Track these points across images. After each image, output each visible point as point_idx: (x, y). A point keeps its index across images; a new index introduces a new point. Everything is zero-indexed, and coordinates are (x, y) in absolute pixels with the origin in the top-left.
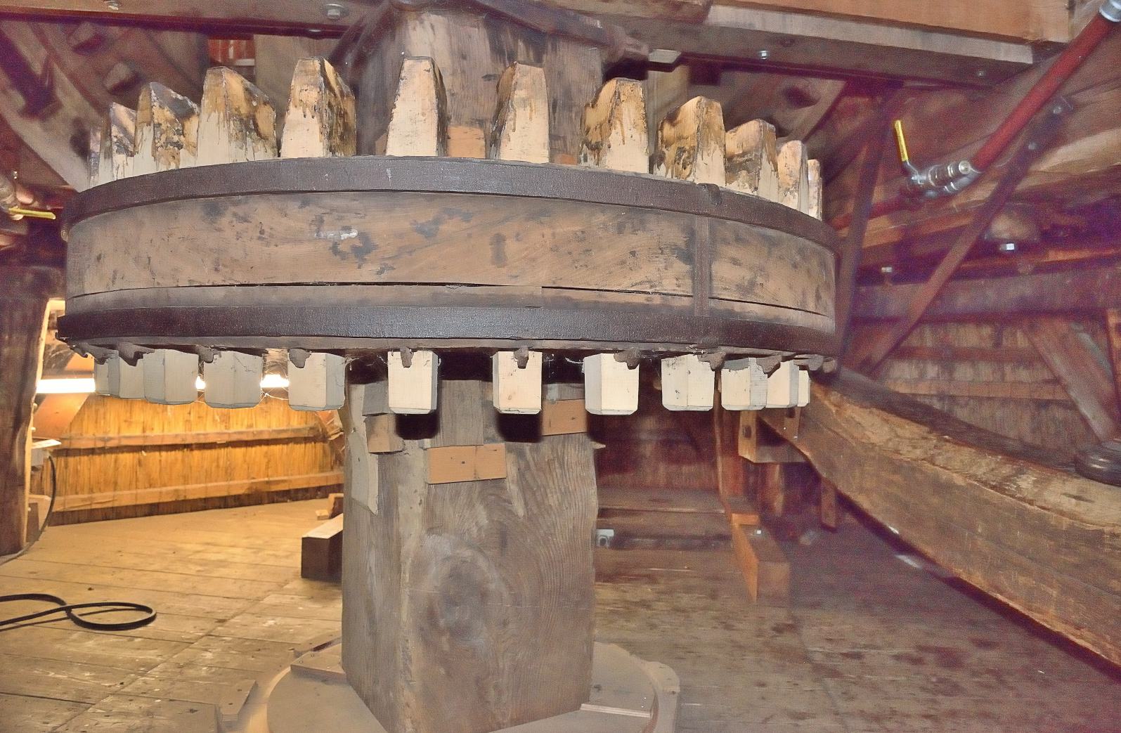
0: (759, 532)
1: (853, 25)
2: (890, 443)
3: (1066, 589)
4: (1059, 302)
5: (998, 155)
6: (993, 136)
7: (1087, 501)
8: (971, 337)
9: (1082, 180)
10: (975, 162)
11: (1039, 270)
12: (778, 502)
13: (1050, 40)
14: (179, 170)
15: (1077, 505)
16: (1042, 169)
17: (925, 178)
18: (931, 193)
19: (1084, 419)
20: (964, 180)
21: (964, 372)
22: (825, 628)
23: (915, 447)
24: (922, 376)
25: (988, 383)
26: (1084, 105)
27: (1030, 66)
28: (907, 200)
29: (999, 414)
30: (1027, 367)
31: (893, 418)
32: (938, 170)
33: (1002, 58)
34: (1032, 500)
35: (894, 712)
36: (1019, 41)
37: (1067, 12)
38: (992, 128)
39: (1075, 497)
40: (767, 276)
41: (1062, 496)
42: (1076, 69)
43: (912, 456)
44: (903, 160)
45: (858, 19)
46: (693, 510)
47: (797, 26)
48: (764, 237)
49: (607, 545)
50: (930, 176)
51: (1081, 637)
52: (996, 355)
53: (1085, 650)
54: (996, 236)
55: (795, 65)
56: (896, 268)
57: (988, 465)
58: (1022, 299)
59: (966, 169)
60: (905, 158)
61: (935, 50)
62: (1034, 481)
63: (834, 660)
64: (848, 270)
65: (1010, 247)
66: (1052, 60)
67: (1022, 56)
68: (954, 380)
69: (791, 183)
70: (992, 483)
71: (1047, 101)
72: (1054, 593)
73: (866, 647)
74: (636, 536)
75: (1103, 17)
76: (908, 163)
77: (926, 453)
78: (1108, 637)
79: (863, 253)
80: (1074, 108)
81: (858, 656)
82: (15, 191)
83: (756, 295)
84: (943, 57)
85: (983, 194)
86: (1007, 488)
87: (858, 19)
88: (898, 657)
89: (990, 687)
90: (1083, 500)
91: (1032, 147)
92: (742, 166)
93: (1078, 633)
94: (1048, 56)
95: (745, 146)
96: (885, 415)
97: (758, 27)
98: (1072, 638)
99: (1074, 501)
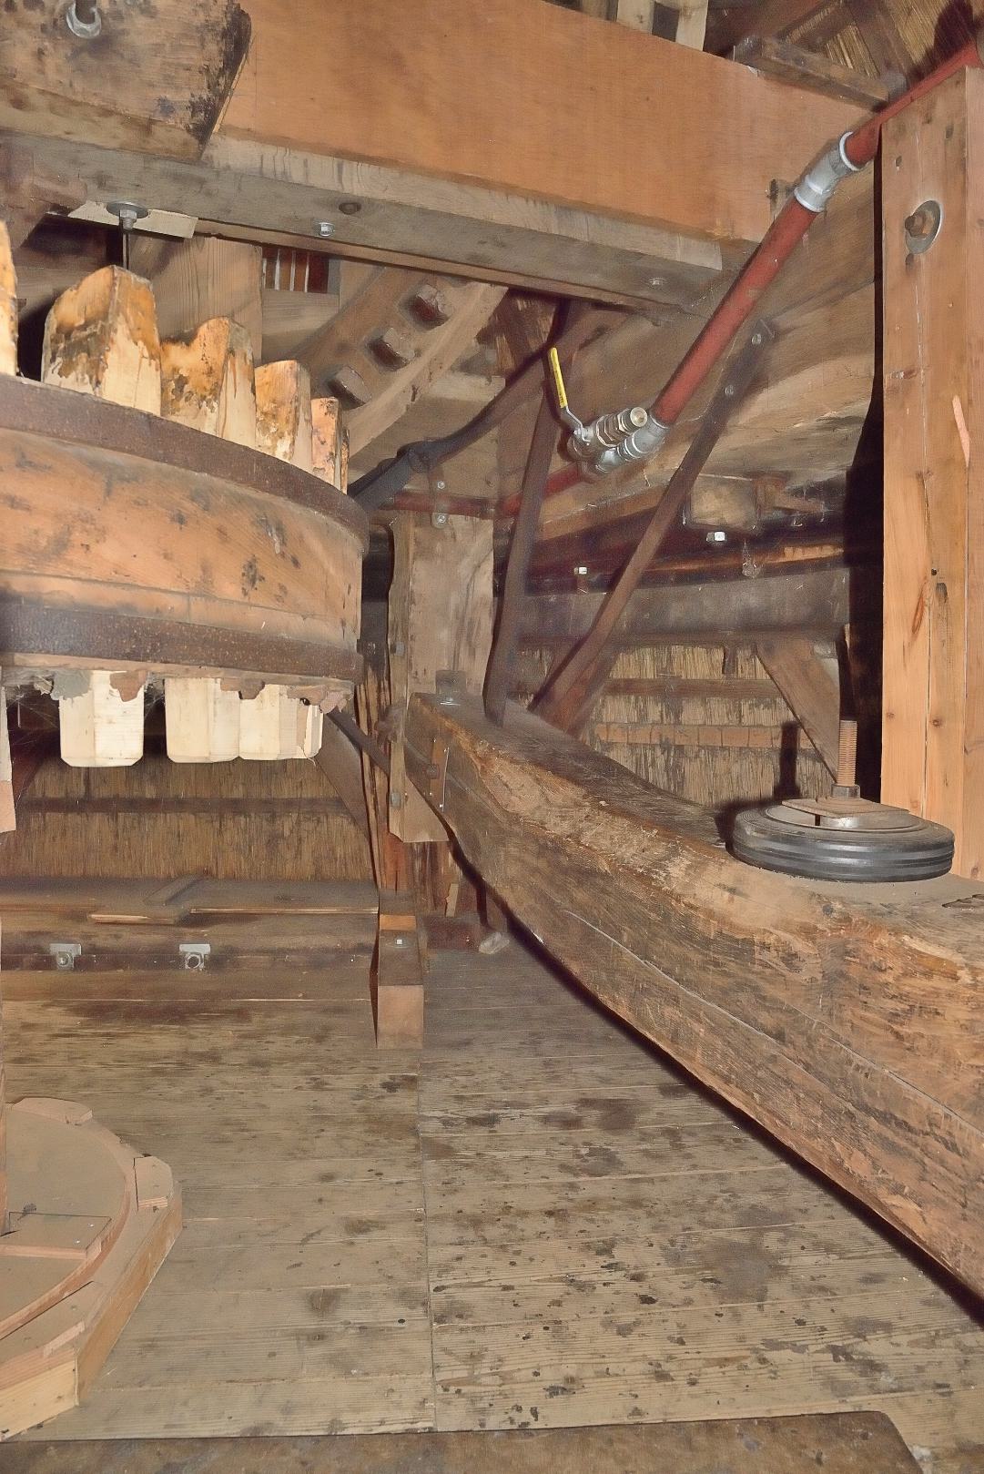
2: (538, 814)
4: (788, 614)
8: (699, 664)
11: (770, 572)
13: (746, 237)
16: (741, 422)
21: (693, 713)
22: (462, 1079)
23: (563, 818)
24: (643, 716)
25: (721, 728)
26: (788, 331)
29: (735, 769)
30: (768, 706)
31: (548, 777)
33: (679, 256)
34: (680, 895)
35: (507, 1209)
37: (769, 201)
40: (103, 533)
43: (558, 831)
46: (334, 910)
47: (359, 182)
48: (95, 465)
49: (201, 966)
51: (731, 1094)
52: (730, 690)
53: (739, 1110)
54: (698, 521)
57: (640, 842)
58: (748, 611)
60: (564, 403)
62: (689, 867)
63: (454, 1129)
65: (720, 537)
68: (680, 723)
69: (208, 387)
73: (508, 1105)
74: (243, 952)
77: (574, 826)
78: (756, 1096)
79: (539, 549)
80: (775, 335)
81: (489, 1121)
83: (70, 563)
84: (592, 248)
86: (655, 876)
87: (459, 179)
88: (546, 1120)
89: (661, 1157)
91: (729, 391)
92: (81, 346)
93: (727, 1088)
95: (89, 310)
96: (539, 772)
97: (297, 176)
98: (724, 1095)
99: (727, 894)
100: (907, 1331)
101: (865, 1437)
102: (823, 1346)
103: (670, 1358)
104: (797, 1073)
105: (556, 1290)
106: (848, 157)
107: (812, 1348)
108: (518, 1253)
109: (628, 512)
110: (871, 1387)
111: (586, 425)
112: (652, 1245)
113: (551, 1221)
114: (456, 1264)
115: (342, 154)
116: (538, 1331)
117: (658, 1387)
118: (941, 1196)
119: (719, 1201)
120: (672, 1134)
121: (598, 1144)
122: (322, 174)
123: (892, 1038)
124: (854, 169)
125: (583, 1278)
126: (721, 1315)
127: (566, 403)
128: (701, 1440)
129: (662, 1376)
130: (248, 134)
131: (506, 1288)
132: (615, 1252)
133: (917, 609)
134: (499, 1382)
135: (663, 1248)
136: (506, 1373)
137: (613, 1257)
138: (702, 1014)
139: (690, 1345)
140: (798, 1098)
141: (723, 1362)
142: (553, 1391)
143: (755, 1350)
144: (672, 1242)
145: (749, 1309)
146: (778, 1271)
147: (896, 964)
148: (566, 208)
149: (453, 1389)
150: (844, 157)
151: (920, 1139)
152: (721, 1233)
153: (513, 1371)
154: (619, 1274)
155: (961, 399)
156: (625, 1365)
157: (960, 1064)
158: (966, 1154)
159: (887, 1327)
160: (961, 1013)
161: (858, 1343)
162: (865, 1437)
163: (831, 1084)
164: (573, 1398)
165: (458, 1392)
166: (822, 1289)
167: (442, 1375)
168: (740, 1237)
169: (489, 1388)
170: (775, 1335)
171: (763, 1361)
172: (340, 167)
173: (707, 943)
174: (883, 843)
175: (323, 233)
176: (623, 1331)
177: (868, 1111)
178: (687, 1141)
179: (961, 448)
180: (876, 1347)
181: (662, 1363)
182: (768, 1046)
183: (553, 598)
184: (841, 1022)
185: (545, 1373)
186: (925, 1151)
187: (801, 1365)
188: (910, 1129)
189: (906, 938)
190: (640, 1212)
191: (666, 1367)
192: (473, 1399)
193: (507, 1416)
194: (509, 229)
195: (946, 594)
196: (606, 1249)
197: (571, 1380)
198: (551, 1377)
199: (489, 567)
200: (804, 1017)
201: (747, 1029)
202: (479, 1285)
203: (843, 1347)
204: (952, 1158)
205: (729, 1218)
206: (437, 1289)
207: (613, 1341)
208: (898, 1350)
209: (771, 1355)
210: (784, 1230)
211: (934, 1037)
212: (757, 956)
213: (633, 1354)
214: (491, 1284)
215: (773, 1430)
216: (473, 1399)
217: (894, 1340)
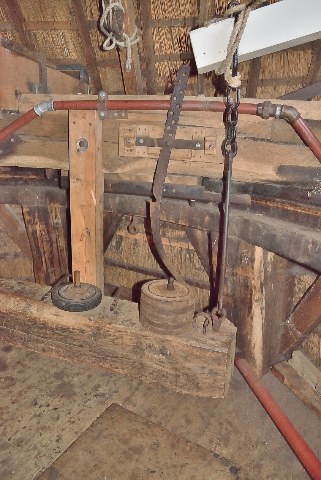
3: (59, 347)
7: (60, 316)
9: (288, 268)
14: (169, 159)
15: (57, 318)
37: (15, 96)
39: (55, 315)
41: (50, 315)
70: (19, 311)
72: (54, 348)
80: (19, 141)
86: (27, 313)
90: (58, 316)
99: (55, 317)
100: (103, 384)
101: (115, 409)
102: (93, 397)
103: (71, 418)
104: (87, 353)
105: (35, 420)
107: (92, 398)
108: (17, 418)
110: (106, 399)
112: (44, 396)
113: (16, 404)
114: (6, 431)
116: (42, 432)
117: (74, 425)
118: (127, 367)
119: (47, 376)
120: (19, 363)
121: (4, 376)
123: (112, 343)
125: (38, 413)
126: (72, 403)
128: (93, 429)
129: (73, 423)
131: (24, 428)
132: (38, 402)
133: (82, 236)
134: (45, 448)
135: (47, 395)
136: (45, 444)
137: (39, 404)
138: (53, 344)
139: (72, 413)
140: (88, 357)
141: (80, 412)
142: (57, 441)
143: (83, 405)
144: (47, 392)
145: (75, 398)
146: (73, 386)
147: (113, 331)
149: (38, 457)
151: (121, 359)
152: (55, 384)
153: (46, 443)
154: (44, 407)
155: (94, 191)
156: (65, 426)
157: (129, 345)
158: (132, 359)
159: (99, 385)
160: (129, 337)
161: (98, 392)
162: (115, 409)
163: (98, 353)
164: (62, 439)
165: (40, 456)
166: (84, 384)
167: (33, 456)
168: (59, 382)
169: (45, 451)
170: (84, 400)
171: (86, 406)
173: (53, 329)
176: (58, 419)
177: (108, 356)
178: (25, 363)
179: (94, 202)
180: (101, 391)
181: (71, 420)
182: (78, 348)
184: (99, 342)
185: (52, 439)
186: (122, 360)
187: (93, 403)
188: (119, 358)
189: (113, 325)
190: (33, 389)
191: (72, 420)
192: (45, 455)
193: (54, 453)
195: (90, 234)
196: (36, 404)
197: (58, 436)
198: (54, 438)
200: (88, 342)
201: (70, 346)
202: (17, 432)
203: (96, 394)
204: (129, 361)
205: (53, 379)
206: (9, 440)
207: (57, 423)
208: (104, 389)
209: (87, 404)
210: (66, 375)
211: (123, 342)
212: (71, 331)
213: (64, 422)
214: (20, 429)
215: (102, 418)
216: (45, 455)
217: (102, 387)
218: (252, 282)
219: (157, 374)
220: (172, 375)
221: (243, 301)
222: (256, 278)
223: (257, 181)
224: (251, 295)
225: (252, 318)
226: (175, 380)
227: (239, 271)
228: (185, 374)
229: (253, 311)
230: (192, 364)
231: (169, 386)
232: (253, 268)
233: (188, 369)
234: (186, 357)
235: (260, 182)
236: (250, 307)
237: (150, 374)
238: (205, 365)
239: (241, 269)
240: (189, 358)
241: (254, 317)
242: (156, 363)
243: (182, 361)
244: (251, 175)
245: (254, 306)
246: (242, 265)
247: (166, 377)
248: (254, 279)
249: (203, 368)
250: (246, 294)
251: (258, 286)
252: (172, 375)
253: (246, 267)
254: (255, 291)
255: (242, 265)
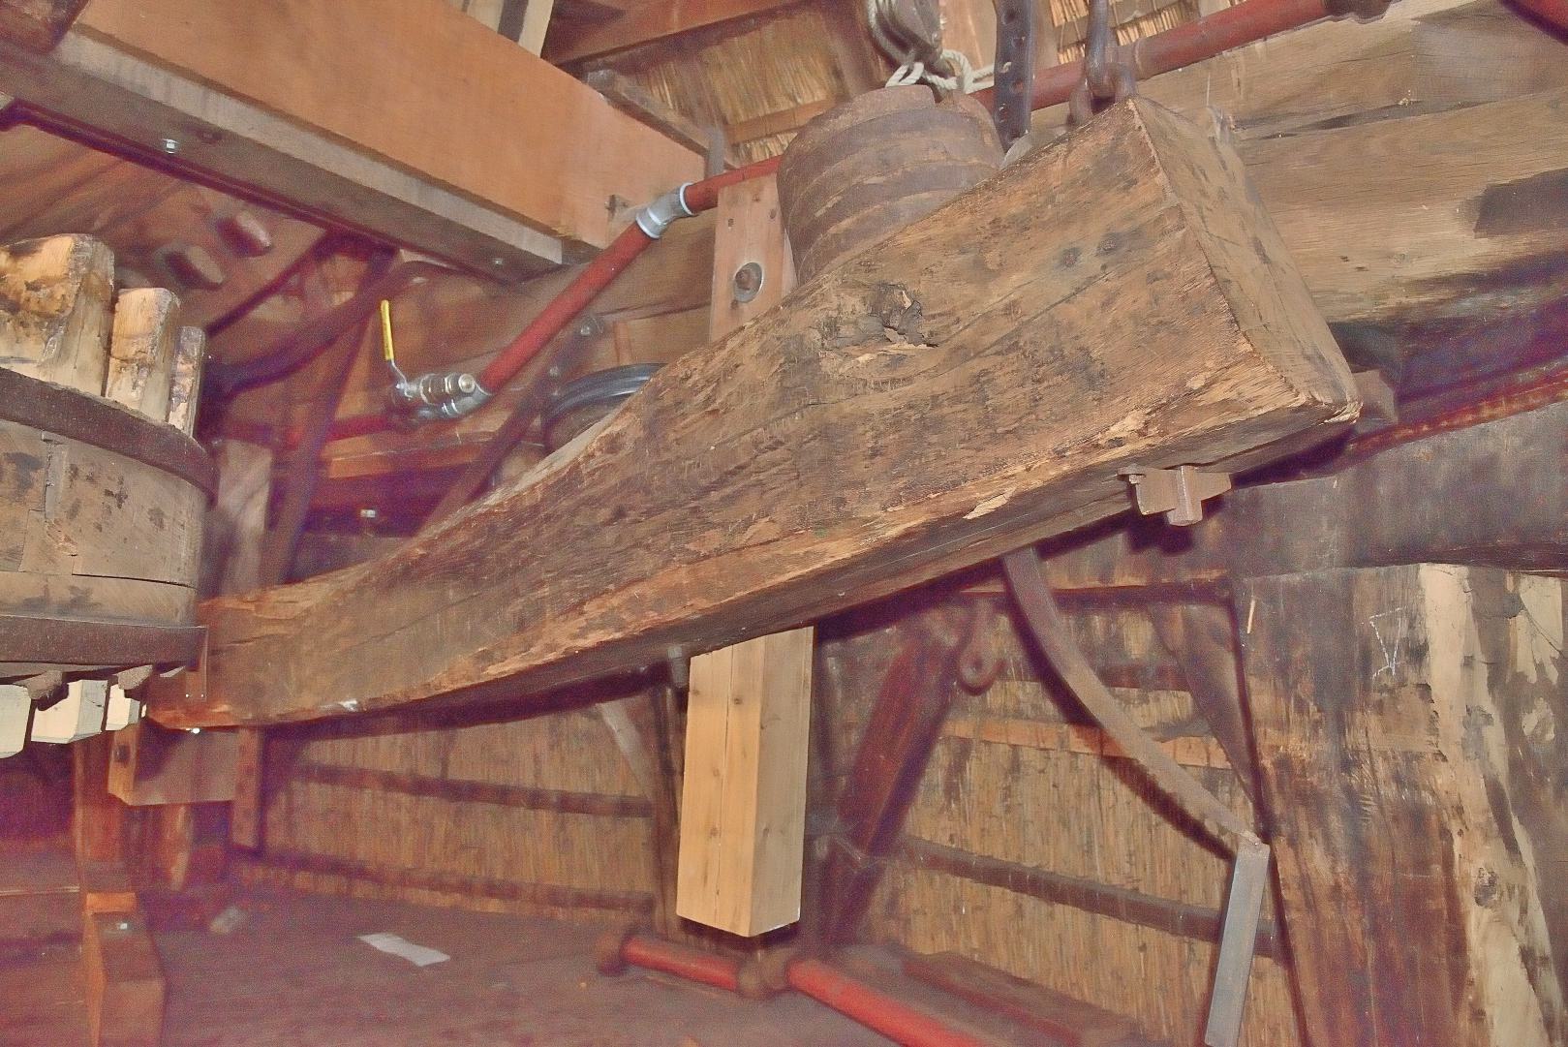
0: (124, 926)
1: (319, 143)
5: (515, 374)
6: (506, 351)
10: (482, 379)
12: (178, 868)
13: (585, 240)
17: (414, 388)
18: (426, 412)
19: (609, 733)
20: (469, 402)
27: (558, 268)
28: (395, 418)
32: (432, 382)
36: (548, 231)
38: (509, 339)
42: (607, 283)
44: (387, 358)
45: (327, 135)
47: (223, 114)
50: (421, 387)
55: (217, 174)
56: (381, 512)
59: (469, 386)
60: (390, 356)
61: (436, 211)
64: (295, 509)
66: (583, 266)
67: (550, 252)
71: (575, 315)
75: (640, 229)
76: (393, 364)
82: (651, 88)
84: (447, 225)
85: (493, 423)
87: (327, 135)
91: (554, 371)
94: (581, 260)
106: (685, 196)
109: (432, 464)
111: (410, 380)
115: (209, 84)
122: (187, 99)
124: (690, 213)
127: (392, 356)
130: (107, 39)
148: (429, 181)
150: (682, 202)
172: (1094, 920)
174: (1114, 85)
175: (168, 149)
183: (333, 538)
194: (370, 191)
199: (262, 498)
218: (1439, 781)
219: (897, 436)
220: (956, 399)
221: (1414, 905)
222: (1452, 751)
223: (1398, 300)
224: (1448, 863)
225: (1478, 1015)
226: (980, 410)
227: (1369, 732)
228: (1009, 350)
229: (1479, 967)
230: (1014, 277)
231: (967, 461)
232: (1425, 689)
233: (1010, 309)
234: (979, 264)
235: (1413, 300)
236: (1458, 945)
237: (873, 456)
238: (1072, 235)
239: (1373, 721)
240: (992, 258)
241: (1488, 1010)
242: (876, 383)
243: (970, 291)
244: (1360, 269)
245: (1473, 936)
246: (1376, 696)
247: (937, 425)
248: (1445, 759)
249: (1069, 258)
250: (1422, 865)
251: (1475, 797)
252: (956, 399)
253: (1395, 699)
254: (1460, 833)
255: (1376, 696)
